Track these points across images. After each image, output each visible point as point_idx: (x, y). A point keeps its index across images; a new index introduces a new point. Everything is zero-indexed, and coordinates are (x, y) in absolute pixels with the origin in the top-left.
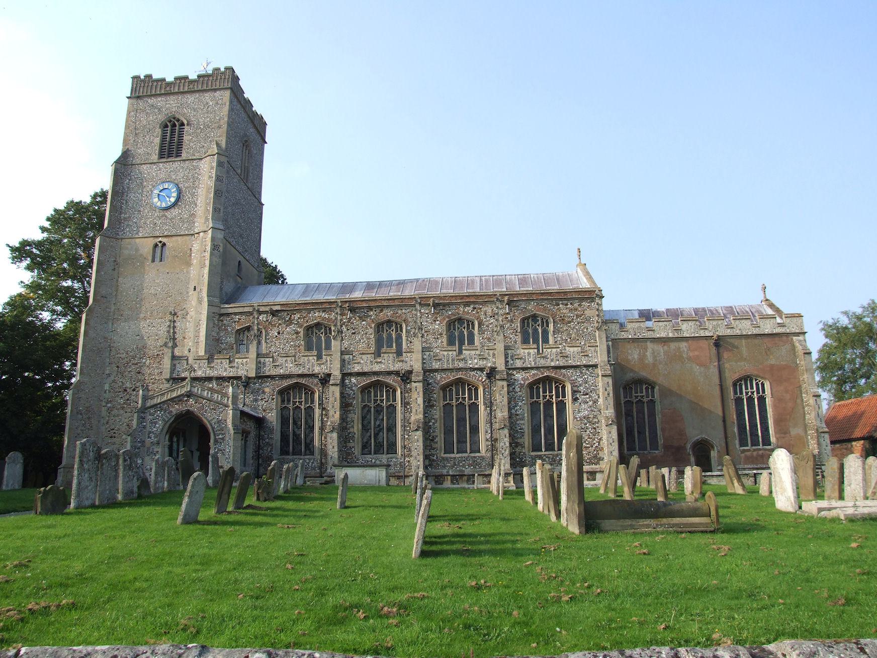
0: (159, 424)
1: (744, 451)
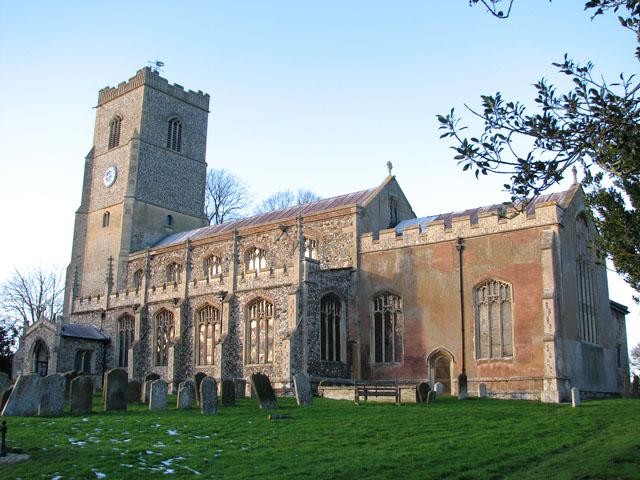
1: (481, 362)
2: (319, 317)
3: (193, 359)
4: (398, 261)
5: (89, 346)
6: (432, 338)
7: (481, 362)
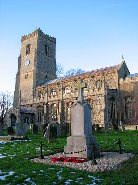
0: (9, 115)
2: (110, 104)
4: (132, 86)
5: (28, 116)
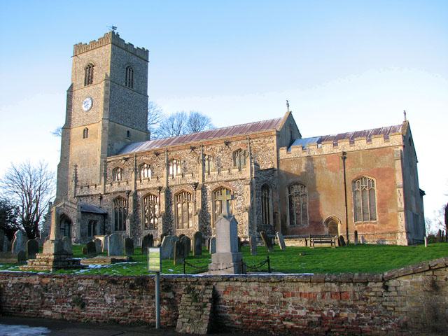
1: (358, 224)
3: (174, 225)
4: (303, 165)
5: (95, 218)
6: (327, 210)
7: (358, 224)
